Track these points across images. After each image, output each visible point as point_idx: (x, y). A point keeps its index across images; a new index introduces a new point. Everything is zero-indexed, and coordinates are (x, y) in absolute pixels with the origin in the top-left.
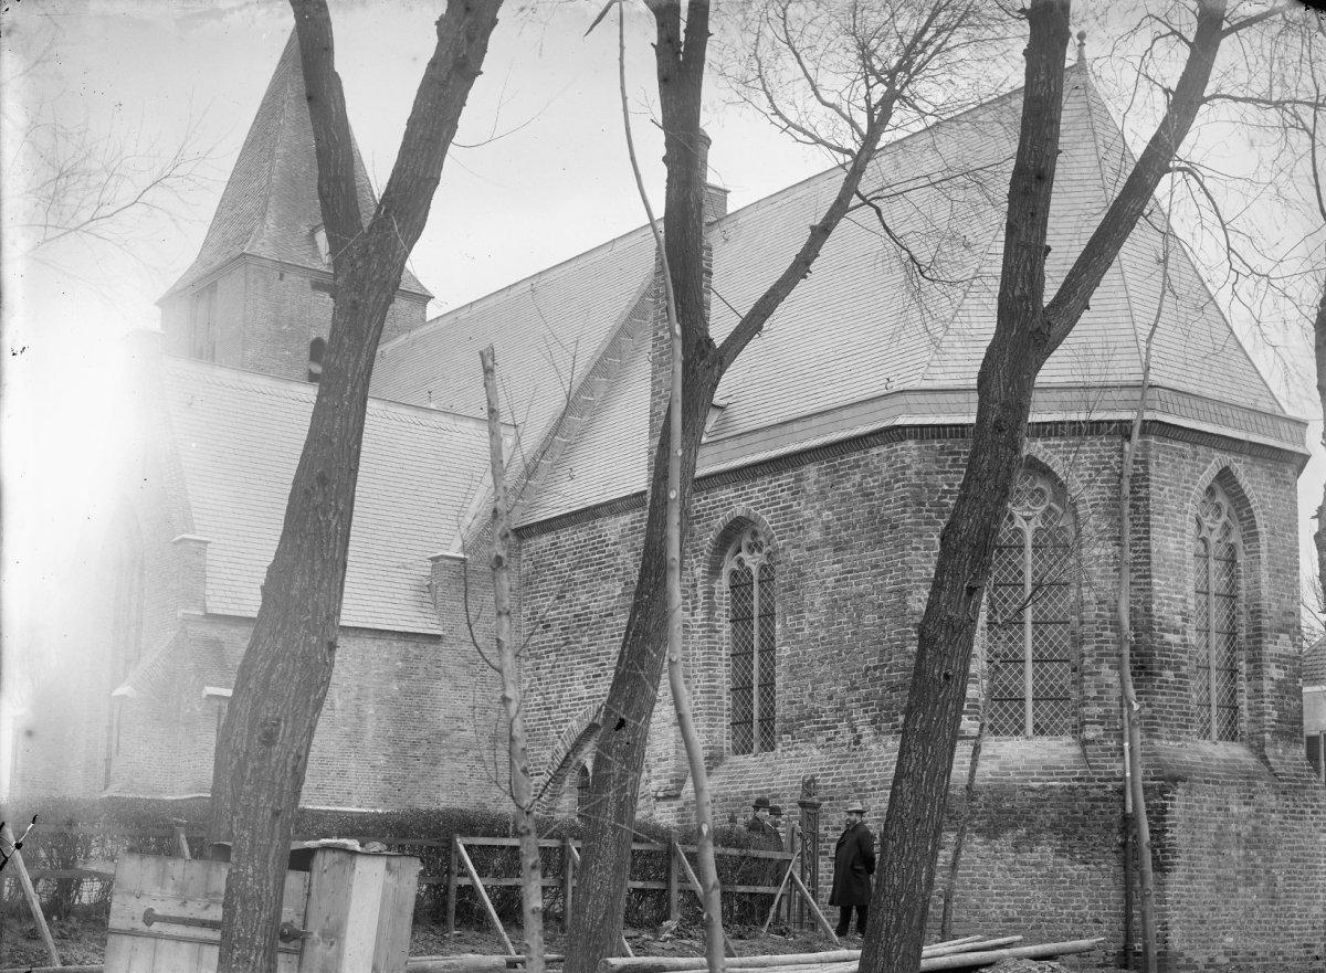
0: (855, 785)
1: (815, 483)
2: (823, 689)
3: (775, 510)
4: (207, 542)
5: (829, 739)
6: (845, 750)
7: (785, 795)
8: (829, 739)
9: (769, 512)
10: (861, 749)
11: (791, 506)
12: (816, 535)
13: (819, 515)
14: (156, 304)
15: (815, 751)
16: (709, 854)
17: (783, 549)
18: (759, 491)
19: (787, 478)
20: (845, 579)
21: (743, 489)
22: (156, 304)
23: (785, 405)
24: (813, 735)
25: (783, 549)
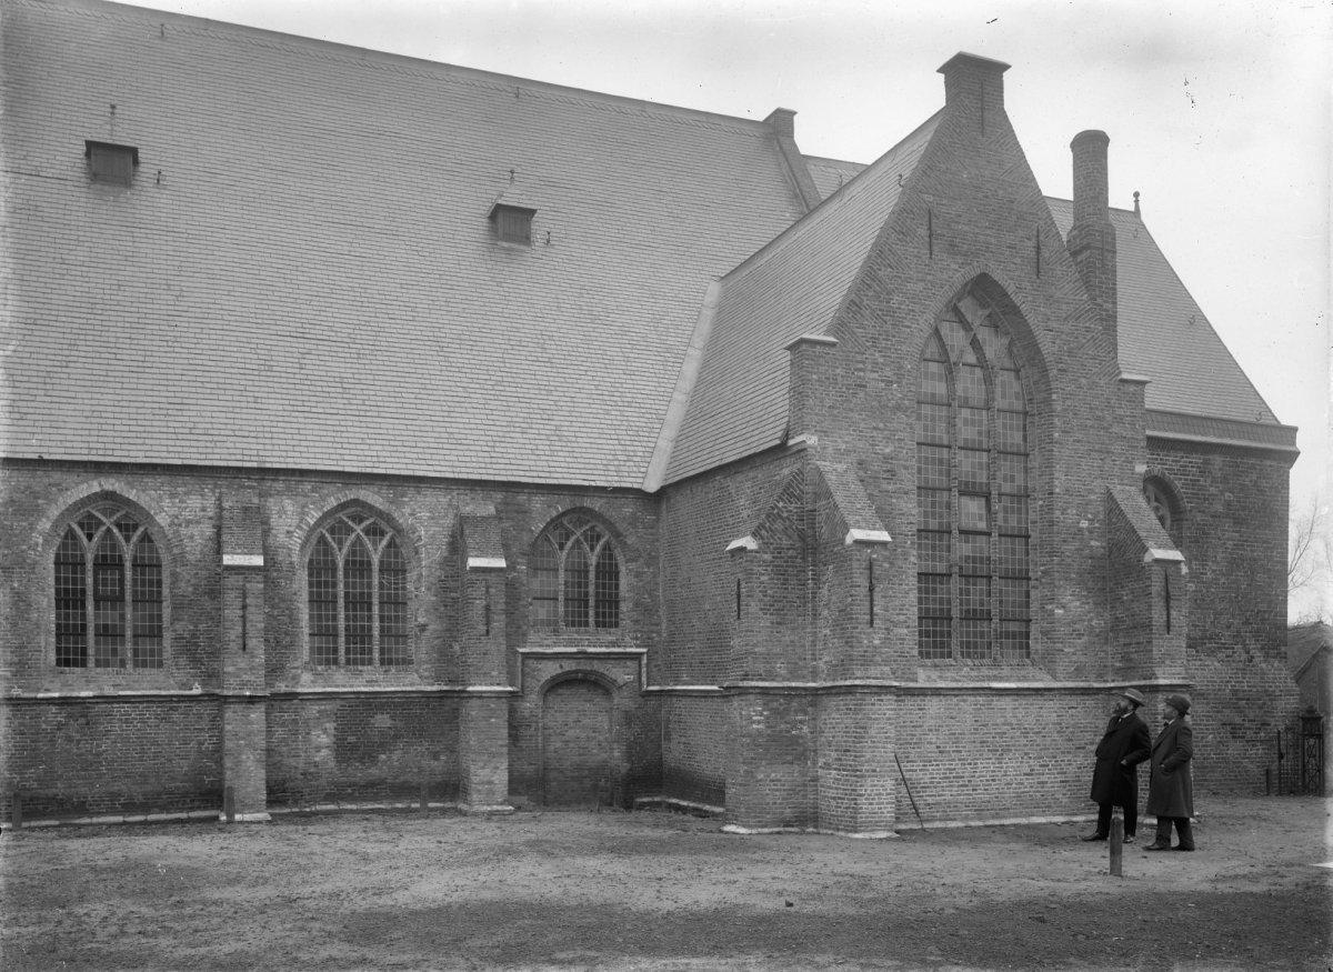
0: (1266, 691)
1: (1220, 469)
2: (1224, 620)
3: (1186, 480)
4: (1143, 383)
5: (1227, 656)
6: (1241, 665)
7: (1209, 694)
8: (1227, 656)
9: (1180, 479)
10: (1253, 666)
11: (1198, 481)
12: (1219, 508)
13: (1222, 494)
14: (938, 71)
15: (1216, 663)
16: (376, 655)
17: (1191, 511)
18: (1173, 461)
19: (1197, 459)
20: (1242, 545)
21: (1158, 455)
22: (938, 71)
23: (410, 380)
24: (1213, 652)
25: (1191, 511)
